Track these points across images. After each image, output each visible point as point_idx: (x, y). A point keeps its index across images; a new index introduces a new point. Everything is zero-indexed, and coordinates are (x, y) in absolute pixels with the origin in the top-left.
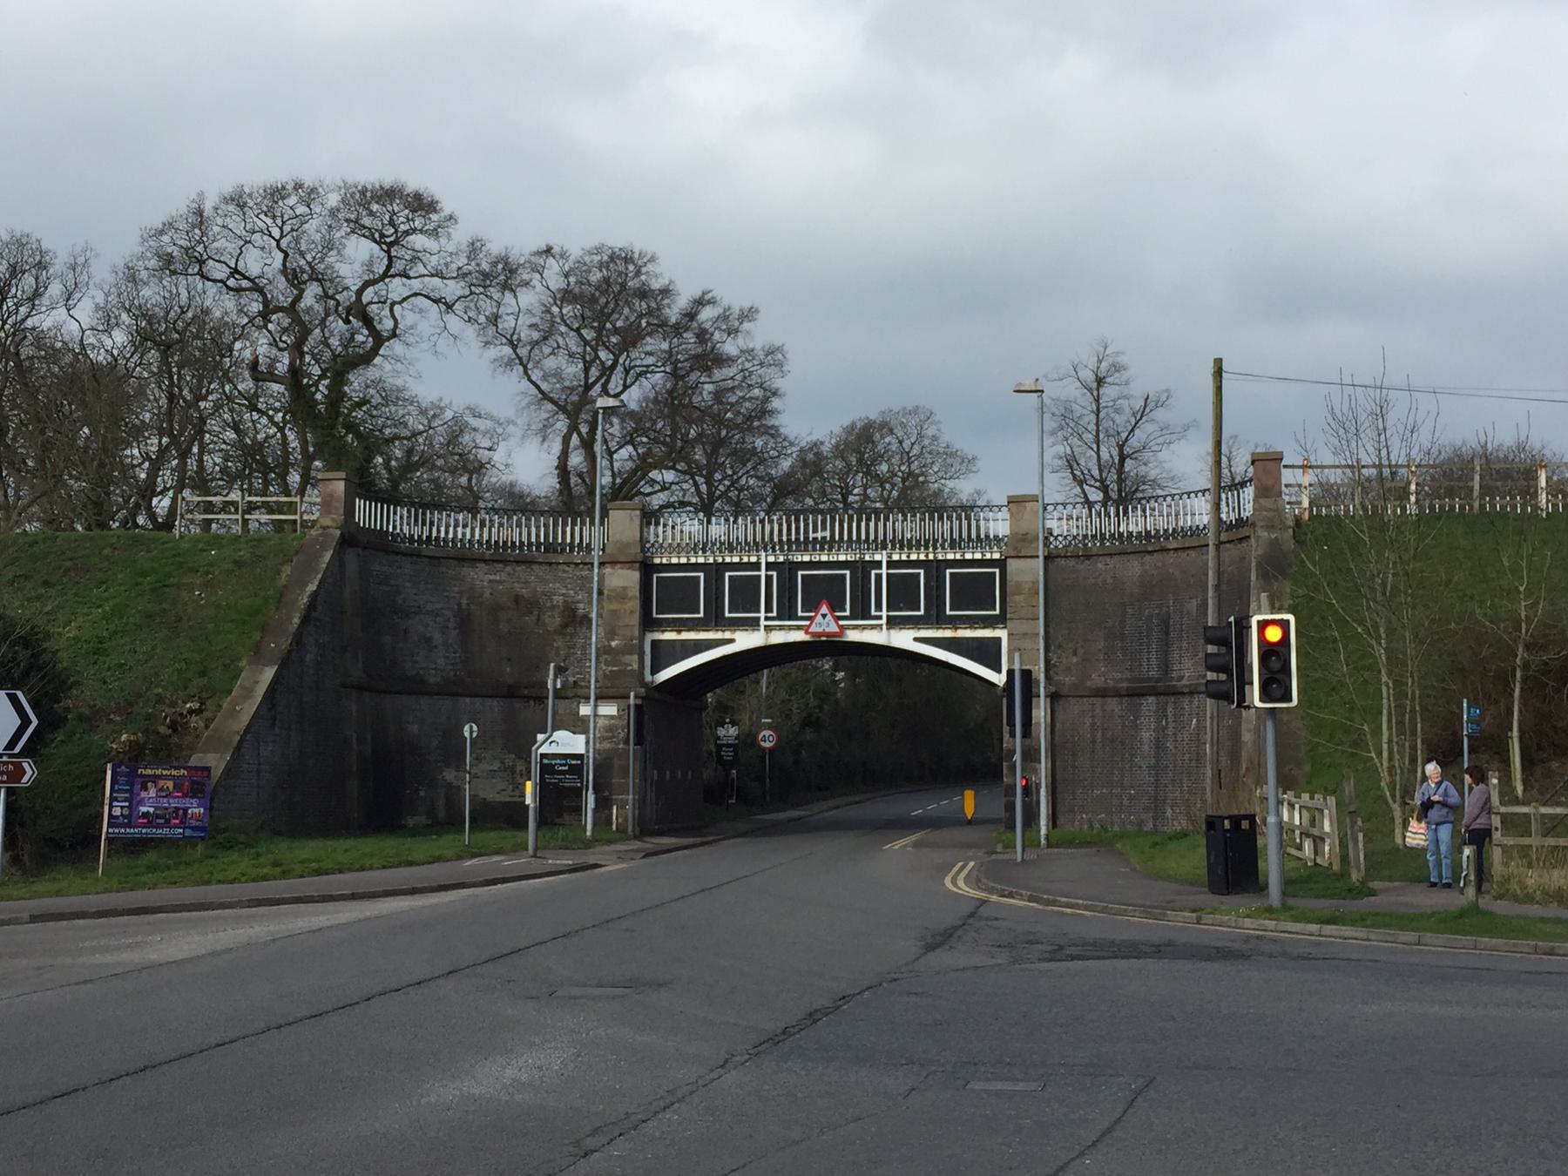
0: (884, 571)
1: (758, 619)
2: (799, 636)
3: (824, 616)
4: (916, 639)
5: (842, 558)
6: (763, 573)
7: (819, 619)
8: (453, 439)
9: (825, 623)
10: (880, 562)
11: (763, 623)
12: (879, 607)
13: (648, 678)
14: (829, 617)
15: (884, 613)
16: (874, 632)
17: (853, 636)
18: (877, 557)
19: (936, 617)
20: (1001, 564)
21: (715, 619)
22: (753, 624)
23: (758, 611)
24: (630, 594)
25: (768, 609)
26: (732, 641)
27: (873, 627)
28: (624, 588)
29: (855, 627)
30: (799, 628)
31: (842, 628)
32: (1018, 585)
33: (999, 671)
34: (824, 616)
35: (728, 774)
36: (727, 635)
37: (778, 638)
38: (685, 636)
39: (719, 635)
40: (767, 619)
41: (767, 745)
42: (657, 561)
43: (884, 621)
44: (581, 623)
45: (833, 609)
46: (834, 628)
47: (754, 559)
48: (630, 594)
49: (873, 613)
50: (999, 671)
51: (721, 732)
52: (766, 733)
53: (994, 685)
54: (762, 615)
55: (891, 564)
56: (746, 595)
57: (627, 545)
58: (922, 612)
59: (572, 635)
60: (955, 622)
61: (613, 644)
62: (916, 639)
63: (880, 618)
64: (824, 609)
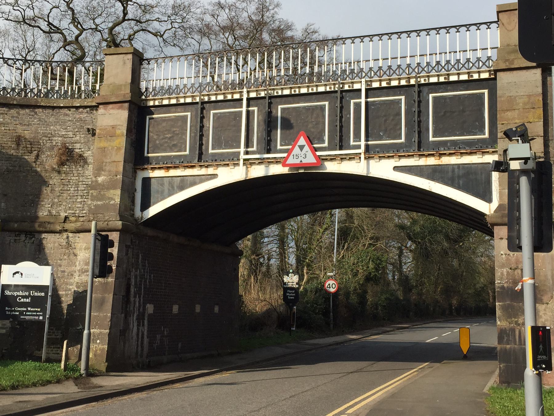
0: (363, 100)
1: (239, 153)
2: (277, 170)
3: (302, 148)
4: (396, 168)
5: (321, 89)
6: (244, 109)
7: (297, 150)
8: (543, 291)
9: (302, 155)
10: (360, 90)
11: (243, 156)
12: (357, 137)
13: (138, 213)
14: (307, 148)
15: (363, 143)
16: (353, 162)
17: (331, 167)
18: (356, 86)
19: (420, 145)
20: (490, 83)
21: (200, 156)
22: (233, 160)
23: (239, 147)
24: (118, 132)
25: (248, 144)
26: (214, 176)
27: (351, 158)
28: (113, 127)
29: (332, 159)
30: (277, 161)
31: (318, 158)
32: (511, 100)
33: (489, 200)
34: (302, 148)
35: (291, 309)
36: (211, 171)
37: (258, 172)
38: (173, 173)
39: (203, 171)
40: (247, 153)
41: (332, 290)
42: (151, 103)
43: (362, 150)
44: (76, 162)
45: (310, 141)
46: (310, 159)
47: (237, 96)
48: (118, 132)
49: (352, 143)
50: (489, 200)
51: (286, 279)
52: (331, 282)
53: (482, 215)
54: (242, 149)
55: (370, 91)
56: (228, 133)
57: (119, 87)
58: (403, 140)
59: (66, 173)
60: (438, 150)
61: (100, 179)
62: (396, 168)
63: (359, 147)
64: (302, 141)
